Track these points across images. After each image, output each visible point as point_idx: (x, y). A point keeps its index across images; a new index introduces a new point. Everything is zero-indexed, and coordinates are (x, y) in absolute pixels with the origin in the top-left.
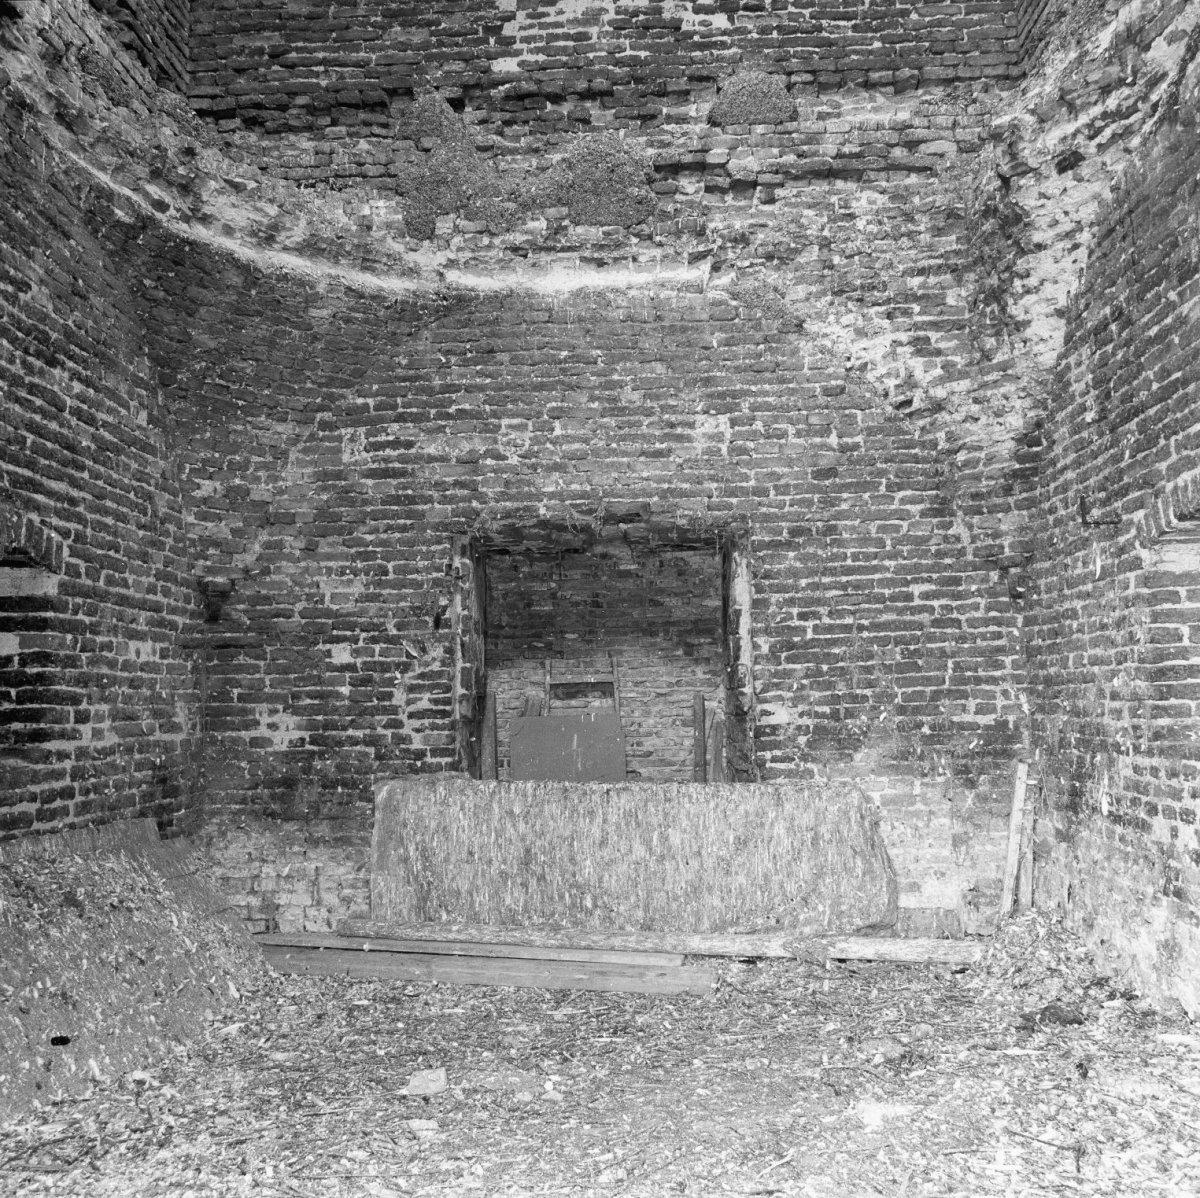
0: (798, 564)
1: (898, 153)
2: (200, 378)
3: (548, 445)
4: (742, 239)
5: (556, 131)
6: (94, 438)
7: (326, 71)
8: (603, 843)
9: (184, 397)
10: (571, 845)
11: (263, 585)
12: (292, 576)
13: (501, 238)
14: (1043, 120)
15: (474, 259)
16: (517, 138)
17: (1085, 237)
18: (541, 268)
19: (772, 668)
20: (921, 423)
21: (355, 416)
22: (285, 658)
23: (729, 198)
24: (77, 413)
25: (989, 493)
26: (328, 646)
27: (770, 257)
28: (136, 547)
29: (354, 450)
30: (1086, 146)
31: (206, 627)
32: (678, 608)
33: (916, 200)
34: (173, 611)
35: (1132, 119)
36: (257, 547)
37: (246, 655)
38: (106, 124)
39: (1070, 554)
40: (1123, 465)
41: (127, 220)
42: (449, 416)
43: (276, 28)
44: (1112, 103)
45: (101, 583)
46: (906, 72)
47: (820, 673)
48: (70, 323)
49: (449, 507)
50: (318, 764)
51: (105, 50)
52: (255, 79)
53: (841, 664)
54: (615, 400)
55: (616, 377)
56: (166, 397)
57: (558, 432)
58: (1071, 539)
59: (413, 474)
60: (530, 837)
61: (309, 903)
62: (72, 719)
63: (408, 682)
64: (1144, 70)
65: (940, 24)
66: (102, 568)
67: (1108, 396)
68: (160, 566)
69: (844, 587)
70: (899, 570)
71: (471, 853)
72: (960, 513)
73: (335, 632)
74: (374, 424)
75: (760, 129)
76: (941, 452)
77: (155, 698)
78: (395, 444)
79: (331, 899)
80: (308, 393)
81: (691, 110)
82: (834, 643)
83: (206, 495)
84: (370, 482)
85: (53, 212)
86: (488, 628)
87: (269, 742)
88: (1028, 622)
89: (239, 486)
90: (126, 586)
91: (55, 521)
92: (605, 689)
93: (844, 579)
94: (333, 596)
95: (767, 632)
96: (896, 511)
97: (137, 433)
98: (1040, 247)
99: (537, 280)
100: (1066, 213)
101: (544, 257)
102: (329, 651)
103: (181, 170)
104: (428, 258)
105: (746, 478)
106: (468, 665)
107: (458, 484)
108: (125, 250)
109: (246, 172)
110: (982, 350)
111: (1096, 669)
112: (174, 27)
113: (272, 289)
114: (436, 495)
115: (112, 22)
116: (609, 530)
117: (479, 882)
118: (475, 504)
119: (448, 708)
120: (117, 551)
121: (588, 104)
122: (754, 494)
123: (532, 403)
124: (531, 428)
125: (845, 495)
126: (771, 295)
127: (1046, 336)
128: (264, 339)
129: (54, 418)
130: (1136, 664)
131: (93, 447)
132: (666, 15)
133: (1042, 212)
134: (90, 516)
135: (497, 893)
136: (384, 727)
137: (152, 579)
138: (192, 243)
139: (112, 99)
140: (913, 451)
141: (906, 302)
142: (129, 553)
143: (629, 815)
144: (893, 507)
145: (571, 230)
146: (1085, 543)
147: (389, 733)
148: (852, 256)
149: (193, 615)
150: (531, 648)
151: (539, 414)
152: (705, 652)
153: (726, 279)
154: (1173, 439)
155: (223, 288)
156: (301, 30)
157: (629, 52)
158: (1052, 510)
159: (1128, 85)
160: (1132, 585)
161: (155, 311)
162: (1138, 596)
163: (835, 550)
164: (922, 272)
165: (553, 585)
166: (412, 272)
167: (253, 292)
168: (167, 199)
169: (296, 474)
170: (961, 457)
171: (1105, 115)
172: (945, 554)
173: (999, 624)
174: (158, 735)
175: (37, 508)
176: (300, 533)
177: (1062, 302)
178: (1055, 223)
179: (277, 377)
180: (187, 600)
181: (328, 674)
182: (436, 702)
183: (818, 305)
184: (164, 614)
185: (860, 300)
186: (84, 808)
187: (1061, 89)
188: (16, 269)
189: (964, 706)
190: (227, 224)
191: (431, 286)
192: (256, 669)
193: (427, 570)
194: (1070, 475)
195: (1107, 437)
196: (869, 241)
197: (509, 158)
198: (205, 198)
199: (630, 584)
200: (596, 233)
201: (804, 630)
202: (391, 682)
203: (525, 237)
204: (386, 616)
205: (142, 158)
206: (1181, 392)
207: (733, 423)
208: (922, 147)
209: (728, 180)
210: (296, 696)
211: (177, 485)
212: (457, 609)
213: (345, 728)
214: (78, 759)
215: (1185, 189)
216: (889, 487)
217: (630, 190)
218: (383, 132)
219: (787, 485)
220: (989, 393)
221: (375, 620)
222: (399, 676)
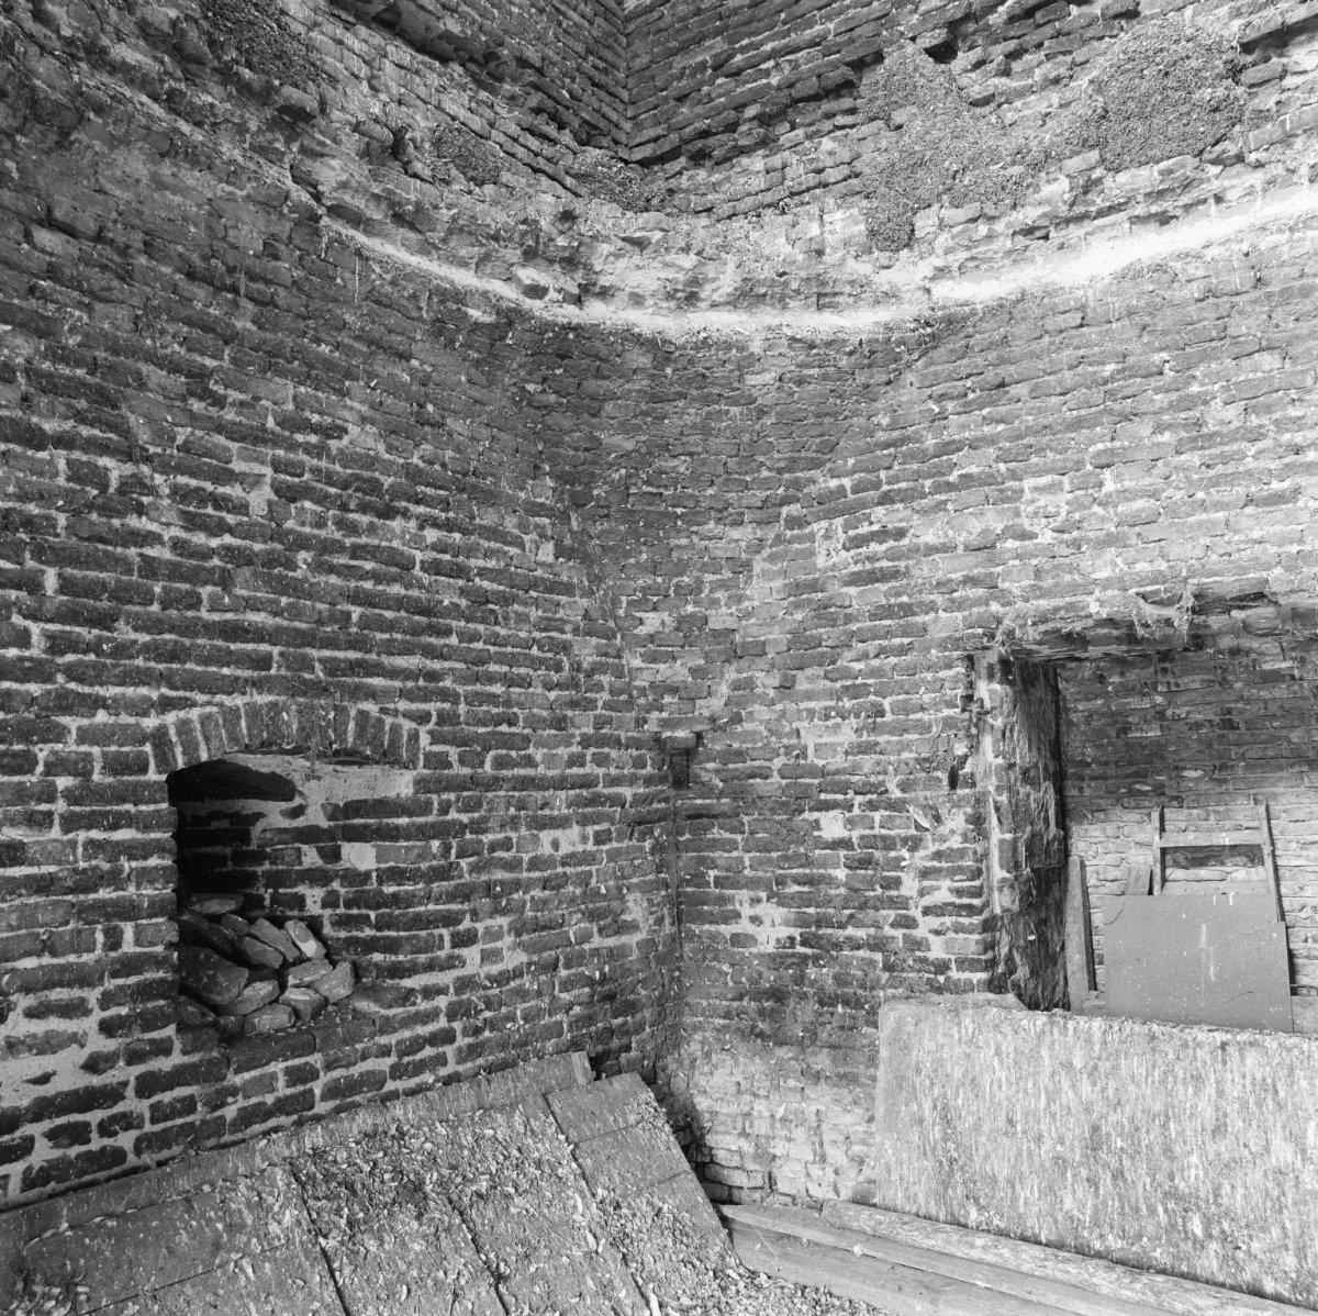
3: (1096, 509)
5: (1084, 42)
7: (777, 64)
8: (1219, 1130)
9: (607, 516)
10: (1165, 1126)
13: (1004, 220)
15: (973, 259)
16: (1029, 72)
18: (1073, 248)
21: (830, 504)
22: (765, 830)
24: (434, 568)
26: (816, 815)
29: (830, 551)
31: (672, 793)
34: (615, 781)
36: (724, 689)
38: (455, 211)
41: (488, 319)
42: (950, 487)
43: (719, 32)
45: (488, 767)
48: (415, 460)
49: (959, 615)
50: (812, 972)
54: (1199, 424)
55: (1195, 389)
57: (1110, 486)
59: (906, 574)
60: (1099, 1108)
61: (811, 1158)
62: (447, 944)
71: (1010, 1122)
73: (823, 796)
78: (882, 535)
79: (836, 1155)
80: (765, 484)
83: (652, 630)
84: (853, 590)
89: (692, 615)
91: (403, 705)
94: (818, 748)
97: (539, 573)
101: (1075, 231)
103: (561, 241)
104: (908, 272)
107: (970, 581)
108: (495, 356)
109: (647, 222)
112: (605, 72)
113: (691, 362)
114: (939, 599)
117: (1025, 1168)
118: (995, 607)
123: (1066, 450)
124: (1067, 487)
128: (694, 425)
129: (394, 580)
131: (464, 603)
134: (460, 690)
135: (1051, 1188)
138: (576, 328)
142: (534, 723)
143: (1267, 1088)
145: (1108, 182)
147: (899, 933)
149: (648, 781)
150: (1132, 793)
155: (630, 374)
156: (748, 23)
165: (1159, 699)
166: (891, 296)
167: (669, 371)
169: (764, 589)
174: (597, 941)
175: (372, 694)
176: (773, 666)
179: (720, 470)
181: (817, 852)
182: (959, 892)
184: (599, 788)
186: (473, 1051)
188: (321, 413)
190: (635, 296)
191: (905, 312)
192: (733, 846)
197: (1018, 104)
198: (598, 268)
199: (1281, 691)
200: (1145, 177)
202: (896, 864)
205: (510, 239)
210: (781, 882)
211: (611, 624)
213: (842, 926)
214: (458, 991)
217: (1196, 96)
218: (849, 120)
221: (872, 779)
222: (906, 855)
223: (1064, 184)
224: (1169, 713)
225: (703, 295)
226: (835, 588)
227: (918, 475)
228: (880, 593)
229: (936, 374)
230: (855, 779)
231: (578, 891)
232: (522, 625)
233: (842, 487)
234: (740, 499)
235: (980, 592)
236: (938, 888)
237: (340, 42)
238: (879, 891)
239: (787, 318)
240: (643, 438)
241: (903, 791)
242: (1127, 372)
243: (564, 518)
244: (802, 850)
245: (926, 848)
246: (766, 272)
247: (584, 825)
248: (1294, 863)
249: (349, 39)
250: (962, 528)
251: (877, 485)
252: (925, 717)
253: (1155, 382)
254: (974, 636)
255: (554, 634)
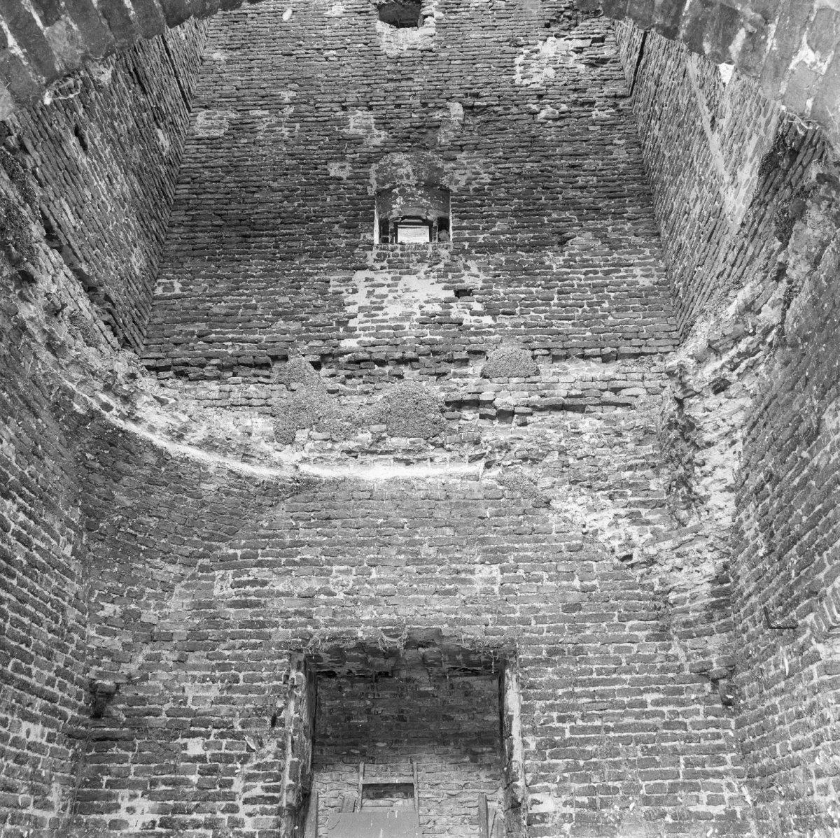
0: (555, 677)
1: (608, 395)
2: (117, 527)
3: (366, 585)
4: (505, 447)
5: (380, 381)
6: (27, 556)
11: (141, 689)
12: (164, 682)
13: (340, 444)
14: (700, 361)
15: (321, 458)
16: (354, 386)
17: (738, 435)
18: (367, 465)
19: (540, 763)
20: (640, 572)
21: (226, 562)
23: (496, 422)
24: (18, 535)
25: (696, 621)
26: (185, 740)
27: (525, 459)
28: (44, 646)
30: (730, 375)
31: (91, 722)
32: (468, 725)
33: (623, 423)
35: (757, 356)
36: (141, 659)
37: (119, 746)
39: (764, 660)
40: (791, 582)
41: (81, 412)
42: (295, 563)
44: (742, 346)
45: (9, 668)
46: (608, 350)
47: (577, 768)
48: (26, 472)
51: (89, 317)
52: (187, 349)
53: (594, 760)
54: (417, 553)
55: (417, 537)
56: (89, 539)
57: (374, 576)
58: (762, 649)
59: (265, 605)
63: (246, 771)
64: (760, 324)
65: (627, 323)
66: (12, 656)
67: (772, 535)
68: (61, 665)
69: (592, 695)
70: (634, 682)
72: (676, 638)
73: (192, 729)
74: (239, 568)
75: (515, 380)
76: (657, 593)
77: (35, 776)
78: (254, 583)
80: (194, 544)
81: (469, 370)
82: (588, 741)
84: (232, 610)
85: (30, 398)
86: (317, 738)
87: (124, 823)
88: (740, 724)
89: (133, 610)
90: (29, 673)
92: (407, 789)
93: (592, 689)
95: (534, 731)
96: (627, 636)
97: (62, 560)
98: (710, 444)
99: (364, 472)
100: (724, 420)
101: (369, 458)
102: (185, 745)
103: (125, 387)
104: (289, 456)
105: (514, 611)
106: (296, 759)
110: (679, 520)
111: (799, 753)
112: (139, 317)
113: (176, 468)
115: (99, 309)
116: (411, 654)
118: (310, 628)
119: (276, 795)
120: (28, 646)
121: (402, 367)
122: (520, 623)
124: (354, 573)
125: (588, 624)
126: (527, 482)
127: (722, 506)
130: (832, 742)
131: (25, 562)
132: (453, 316)
133: (707, 420)
134: (10, 614)
136: (223, 811)
137: (52, 674)
139: (86, 342)
140: (636, 591)
141: (622, 487)
142: (37, 650)
144: (625, 633)
145: (388, 440)
146: (774, 649)
147: (226, 816)
148: (581, 459)
149: (81, 710)
150: (349, 754)
151: (361, 563)
152: (487, 759)
153: (495, 472)
154: (825, 554)
157: (429, 336)
158: (744, 630)
159: (750, 335)
160: (815, 675)
161: (91, 476)
162: (822, 683)
163: (583, 666)
164: (631, 468)
166: (277, 465)
167: (163, 469)
168: (112, 403)
169: (177, 603)
170: (672, 596)
171: (739, 354)
172: (668, 670)
173: (717, 727)
174: (31, 810)
177: (731, 480)
178: (717, 427)
179: (172, 530)
180: (79, 698)
181: (182, 764)
182: (267, 789)
183: (560, 490)
184: (57, 704)
185: (589, 487)
187: (709, 341)
189: (698, 797)
191: (287, 473)
192: (125, 759)
193: (269, 679)
194: (754, 599)
195: (777, 564)
196: (593, 448)
197: (349, 397)
198: (138, 406)
199: (427, 703)
200: (404, 442)
201: (563, 730)
202: (232, 772)
203: (357, 444)
204: (233, 716)
205: (100, 377)
206: (824, 518)
207: (503, 570)
208: (623, 391)
209: (495, 411)
211: (86, 605)
212: (293, 712)
213: (190, 813)
215: (800, 384)
216: (620, 618)
217: (428, 416)
218: (266, 380)
219: (544, 617)
220: (687, 549)
222: (239, 766)
223: (369, 435)
224: (373, 710)
225: (186, 437)
226: (221, 608)
227: (279, 555)
228: (247, 614)
229: (297, 506)
230: (215, 719)
231: (30, 770)
232: (46, 587)
233: (235, 555)
234: (178, 549)
235: (303, 619)
236: (255, 787)
237: (47, 254)
238: (218, 788)
239: (226, 461)
240: (137, 501)
241: (243, 727)
242: (388, 524)
243: (80, 533)
244: (172, 762)
245: (252, 762)
246: (221, 436)
247: (45, 726)
248: (427, 796)
249: (51, 254)
250: (298, 584)
251: (255, 556)
252: (262, 684)
253: (399, 531)
254: (296, 642)
255: (60, 599)
